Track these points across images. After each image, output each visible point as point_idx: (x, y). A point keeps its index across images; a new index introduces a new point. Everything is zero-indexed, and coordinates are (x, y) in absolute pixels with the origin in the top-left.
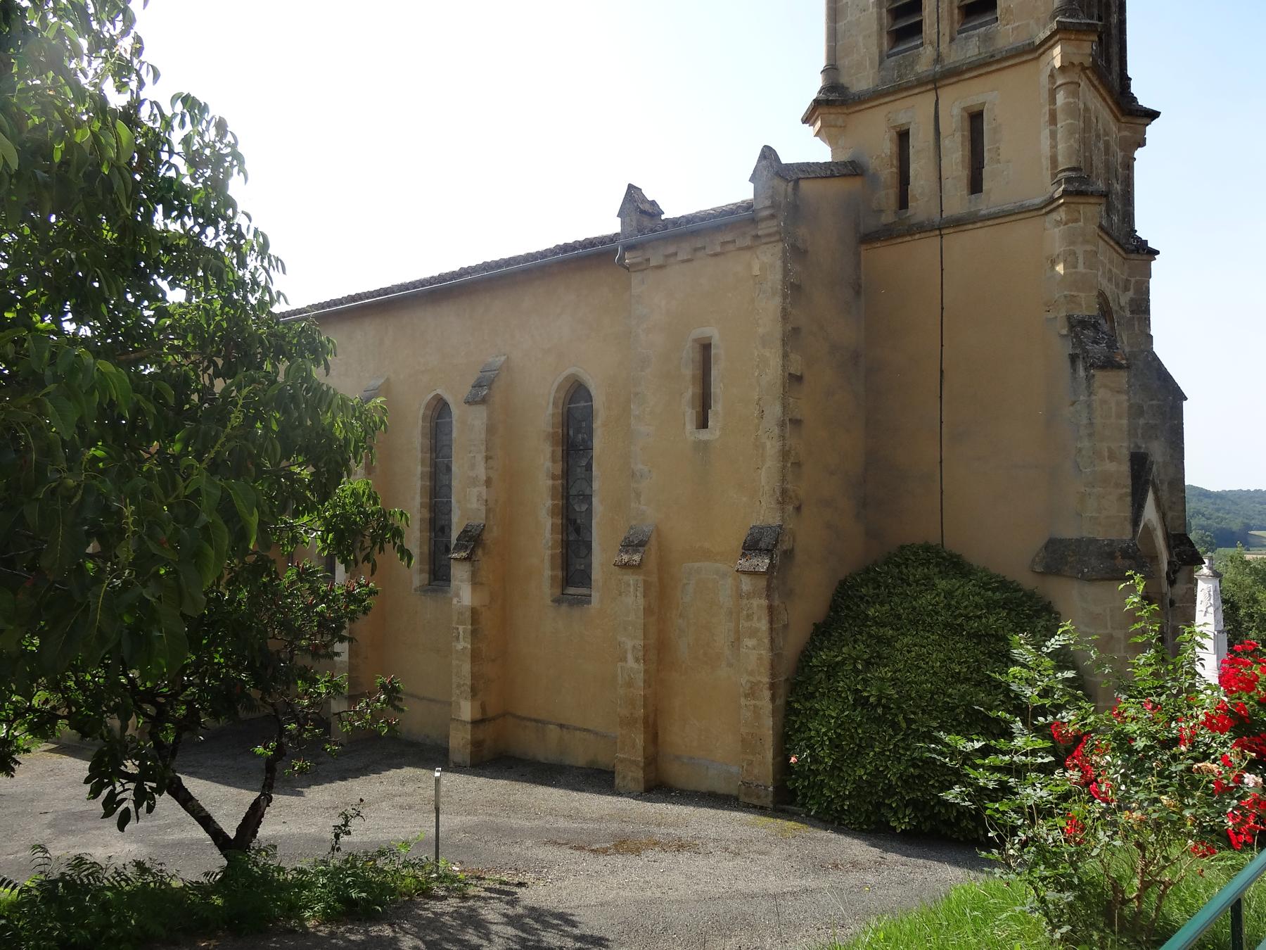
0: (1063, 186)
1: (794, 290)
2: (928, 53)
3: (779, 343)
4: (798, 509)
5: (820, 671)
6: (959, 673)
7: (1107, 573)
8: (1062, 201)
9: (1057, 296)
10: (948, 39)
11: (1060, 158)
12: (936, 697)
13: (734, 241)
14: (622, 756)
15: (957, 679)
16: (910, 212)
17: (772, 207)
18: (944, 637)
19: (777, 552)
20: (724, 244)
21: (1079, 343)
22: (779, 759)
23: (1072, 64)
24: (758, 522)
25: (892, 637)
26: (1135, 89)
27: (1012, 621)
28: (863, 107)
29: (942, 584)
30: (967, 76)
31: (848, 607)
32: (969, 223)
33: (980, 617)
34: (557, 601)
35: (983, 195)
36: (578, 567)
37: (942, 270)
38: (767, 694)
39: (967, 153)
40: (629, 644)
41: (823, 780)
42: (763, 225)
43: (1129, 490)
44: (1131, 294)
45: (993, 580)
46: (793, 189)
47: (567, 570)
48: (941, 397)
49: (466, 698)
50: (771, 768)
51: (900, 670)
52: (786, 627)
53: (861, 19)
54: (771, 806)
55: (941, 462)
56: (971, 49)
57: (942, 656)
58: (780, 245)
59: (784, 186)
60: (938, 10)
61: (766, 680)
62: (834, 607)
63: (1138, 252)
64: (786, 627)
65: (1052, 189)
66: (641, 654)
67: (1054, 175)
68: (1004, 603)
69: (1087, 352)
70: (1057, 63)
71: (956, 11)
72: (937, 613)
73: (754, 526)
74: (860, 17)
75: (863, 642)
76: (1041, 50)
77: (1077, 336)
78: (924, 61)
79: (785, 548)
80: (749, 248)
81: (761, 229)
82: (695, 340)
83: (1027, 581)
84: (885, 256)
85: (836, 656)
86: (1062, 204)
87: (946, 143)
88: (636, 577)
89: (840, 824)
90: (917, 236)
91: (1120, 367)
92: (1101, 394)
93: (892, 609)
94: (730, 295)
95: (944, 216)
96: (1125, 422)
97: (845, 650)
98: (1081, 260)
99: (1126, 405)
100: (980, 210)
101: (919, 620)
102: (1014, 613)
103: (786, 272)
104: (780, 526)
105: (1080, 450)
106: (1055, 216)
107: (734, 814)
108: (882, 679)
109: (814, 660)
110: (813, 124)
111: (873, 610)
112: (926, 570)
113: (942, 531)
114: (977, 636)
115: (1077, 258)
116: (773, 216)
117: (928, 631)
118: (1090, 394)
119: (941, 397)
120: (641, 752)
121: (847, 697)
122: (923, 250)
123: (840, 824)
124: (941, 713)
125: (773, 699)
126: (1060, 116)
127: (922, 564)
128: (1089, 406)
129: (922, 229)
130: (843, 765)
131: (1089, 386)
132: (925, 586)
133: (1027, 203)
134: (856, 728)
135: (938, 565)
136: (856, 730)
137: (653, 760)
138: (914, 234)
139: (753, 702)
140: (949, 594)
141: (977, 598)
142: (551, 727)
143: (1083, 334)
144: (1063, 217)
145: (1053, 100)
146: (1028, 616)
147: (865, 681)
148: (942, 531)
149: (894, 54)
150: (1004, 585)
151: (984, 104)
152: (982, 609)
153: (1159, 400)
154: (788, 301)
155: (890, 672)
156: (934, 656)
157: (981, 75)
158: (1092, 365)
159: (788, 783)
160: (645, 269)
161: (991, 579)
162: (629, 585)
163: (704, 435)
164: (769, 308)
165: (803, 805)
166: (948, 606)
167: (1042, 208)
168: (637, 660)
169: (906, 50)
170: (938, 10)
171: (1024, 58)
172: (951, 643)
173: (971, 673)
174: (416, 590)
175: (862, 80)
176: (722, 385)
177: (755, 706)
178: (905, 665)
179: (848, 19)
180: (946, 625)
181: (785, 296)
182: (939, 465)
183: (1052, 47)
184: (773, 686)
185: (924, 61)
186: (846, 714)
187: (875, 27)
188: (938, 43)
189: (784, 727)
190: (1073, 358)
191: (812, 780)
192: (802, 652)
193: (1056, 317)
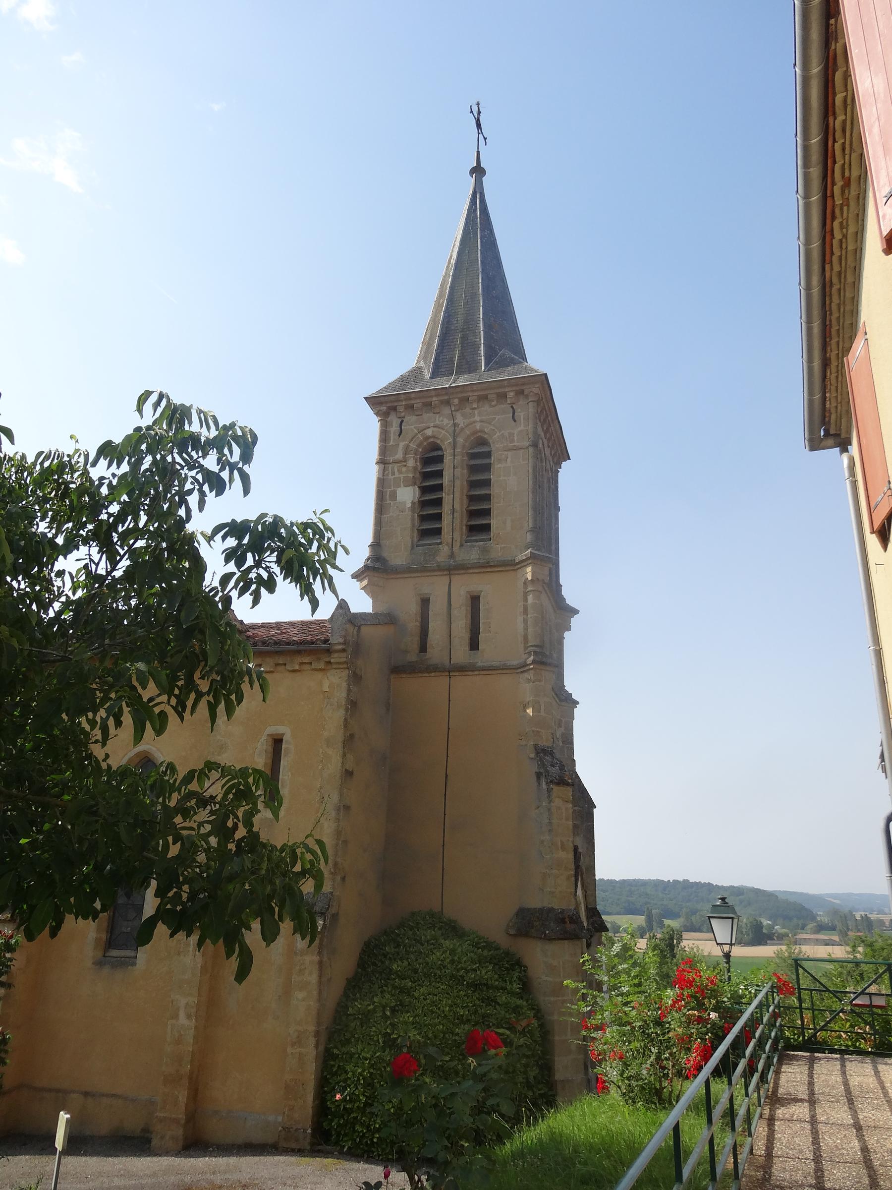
0: (532, 657)
1: (352, 705)
2: (445, 550)
3: (340, 745)
4: (343, 879)
5: (355, 1019)
6: (462, 1016)
7: (561, 934)
8: (532, 667)
9: (527, 730)
10: (459, 544)
11: (529, 637)
12: (447, 1036)
14: (162, 1115)
15: (462, 1020)
16: (428, 655)
17: (344, 643)
18: (451, 987)
19: (328, 915)
20: (302, 664)
21: (542, 765)
22: (317, 1102)
23: (538, 579)
25: (411, 988)
26: (565, 592)
27: (496, 973)
29: (447, 943)
30: (471, 571)
31: (374, 964)
32: (470, 671)
33: (475, 970)
34: (99, 964)
36: (124, 930)
38: (312, 1041)
39: (469, 622)
40: (183, 1001)
41: (355, 1118)
42: (336, 655)
43: (573, 873)
44: (562, 729)
45: (482, 940)
46: (357, 632)
47: (111, 932)
50: (311, 1110)
51: (418, 1015)
52: (329, 980)
53: (400, 517)
54: (308, 1148)
55: (443, 845)
56: (472, 554)
57: (450, 1002)
58: (346, 672)
59: (352, 630)
60: (453, 524)
61: (312, 1028)
62: (362, 964)
63: (567, 702)
64: (329, 980)
65: (526, 656)
66: (194, 1010)
67: (526, 648)
68: (491, 959)
69: (548, 771)
70: (530, 578)
71: (464, 527)
72: (444, 967)
73: (308, 893)
74: (399, 515)
75: (388, 992)
76: (519, 566)
77: (541, 760)
78: (442, 556)
79: (333, 912)
80: (322, 670)
81: (333, 658)
82: (268, 735)
83: (502, 940)
84: (411, 685)
85: (369, 1005)
86: (532, 669)
89: (368, 1157)
90: (433, 674)
91: (568, 784)
92: (557, 802)
93: (409, 964)
94: (303, 703)
96: (571, 823)
97: (376, 999)
98: (542, 707)
99: (571, 811)
100: (478, 662)
101: (432, 973)
102: (497, 967)
103: (349, 691)
104: (331, 893)
105: (542, 842)
106: (526, 675)
107: (277, 1158)
108: (406, 1023)
109: (350, 1009)
110: (361, 581)
111: (396, 966)
112: (433, 932)
113: (442, 901)
114: (476, 986)
115: (540, 706)
116: (344, 650)
117: (438, 982)
118: (550, 802)
120: (183, 1108)
121: (378, 1040)
122: (437, 684)
123: (368, 1157)
124: (451, 1050)
125: (317, 1046)
126: (530, 610)
127: (430, 928)
128: (549, 810)
129: (436, 669)
130: (374, 1101)
131: (549, 796)
132: (434, 945)
133: (508, 663)
134: (385, 1067)
135: (440, 929)
136: (385, 1069)
137: (192, 1117)
138: (431, 672)
139: (298, 1050)
140: (453, 952)
141: (472, 955)
143: (545, 759)
144: (532, 677)
145: (526, 600)
146: (507, 968)
147: (393, 1025)
148: (442, 901)
149: (423, 545)
150: (489, 945)
151: (481, 591)
152: (476, 964)
153: (579, 807)
154: (348, 714)
155: (412, 1017)
156: (444, 1002)
158: (551, 781)
159: (324, 1124)
161: (480, 939)
164: (334, 718)
165: (336, 1143)
166: (452, 962)
167: (518, 668)
168: (189, 1017)
169: (430, 544)
170: (453, 524)
171: (507, 568)
172: (455, 991)
173: (471, 1016)
175: (398, 558)
176: (290, 773)
177: (300, 1054)
178: (422, 1011)
179: (391, 514)
180: (452, 977)
181: (347, 710)
183: (526, 566)
184: (317, 1034)
185: (442, 556)
186: (377, 1055)
187: (409, 525)
188: (452, 545)
189: (322, 1072)
190: (539, 775)
191: (346, 1118)
192: (338, 1004)
193: (526, 745)
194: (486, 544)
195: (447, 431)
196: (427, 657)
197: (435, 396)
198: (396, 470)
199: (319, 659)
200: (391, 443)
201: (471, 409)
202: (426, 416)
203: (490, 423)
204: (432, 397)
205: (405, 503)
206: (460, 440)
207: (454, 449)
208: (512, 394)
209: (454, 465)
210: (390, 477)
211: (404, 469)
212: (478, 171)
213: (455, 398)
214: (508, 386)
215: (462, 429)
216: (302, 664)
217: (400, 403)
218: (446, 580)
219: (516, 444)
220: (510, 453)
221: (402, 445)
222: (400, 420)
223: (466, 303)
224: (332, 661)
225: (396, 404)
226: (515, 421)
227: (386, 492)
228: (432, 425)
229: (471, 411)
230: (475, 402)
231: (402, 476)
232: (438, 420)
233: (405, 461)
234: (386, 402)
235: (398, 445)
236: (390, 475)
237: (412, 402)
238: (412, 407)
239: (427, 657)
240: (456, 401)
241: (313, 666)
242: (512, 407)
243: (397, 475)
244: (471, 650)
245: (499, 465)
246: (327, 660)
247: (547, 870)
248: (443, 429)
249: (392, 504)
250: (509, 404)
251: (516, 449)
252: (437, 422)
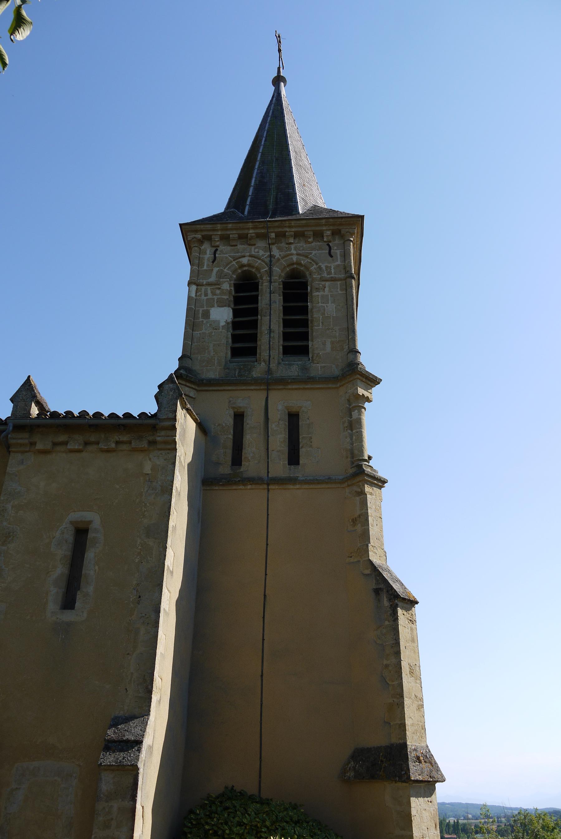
10: (276, 361)
13: (130, 443)
24: (122, 712)
28: (211, 388)
30: (290, 387)
35: (300, 467)
37: (268, 515)
48: (264, 617)
53: (213, 334)
55: (262, 676)
71: (281, 347)
82: (71, 523)
87: (272, 426)
94: (118, 487)
95: (270, 476)
119: (264, 617)
151: (301, 407)
157: (299, 389)
160: (26, 452)
163: (68, 616)
176: (97, 567)
182: (260, 678)
185: (259, 370)
193: (359, 561)
194: (305, 363)
195: (263, 261)
196: (242, 470)
197: (252, 228)
198: (209, 292)
200: (205, 268)
201: (287, 244)
203: (307, 257)
204: (248, 229)
205: (219, 322)
207: (270, 277)
208: (329, 233)
209: (271, 291)
210: (203, 297)
211: (218, 292)
212: (278, 80)
213: (272, 232)
214: (325, 225)
215: (278, 260)
216: (117, 443)
217: (215, 233)
218: (263, 394)
219: (333, 276)
220: (327, 284)
221: (216, 270)
222: (214, 249)
224: (159, 439)
225: (211, 233)
226: (331, 256)
227: (199, 310)
228: (248, 254)
229: (287, 246)
230: (292, 237)
231: (215, 297)
233: (219, 285)
234: (202, 231)
235: (212, 270)
236: (203, 296)
237: (228, 232)
239: (242, 470)
240: (273, 235)
241: (133, 444)
242: (328, 245)
243: (210, 296)
244: (290, 464)
245: (317, 293)
246: (151, 438)
247: (395, 700)
248: (259, 259)
249: (205, 322)
250: (325, 242)
251: (333, 280)
252: (253, 253)
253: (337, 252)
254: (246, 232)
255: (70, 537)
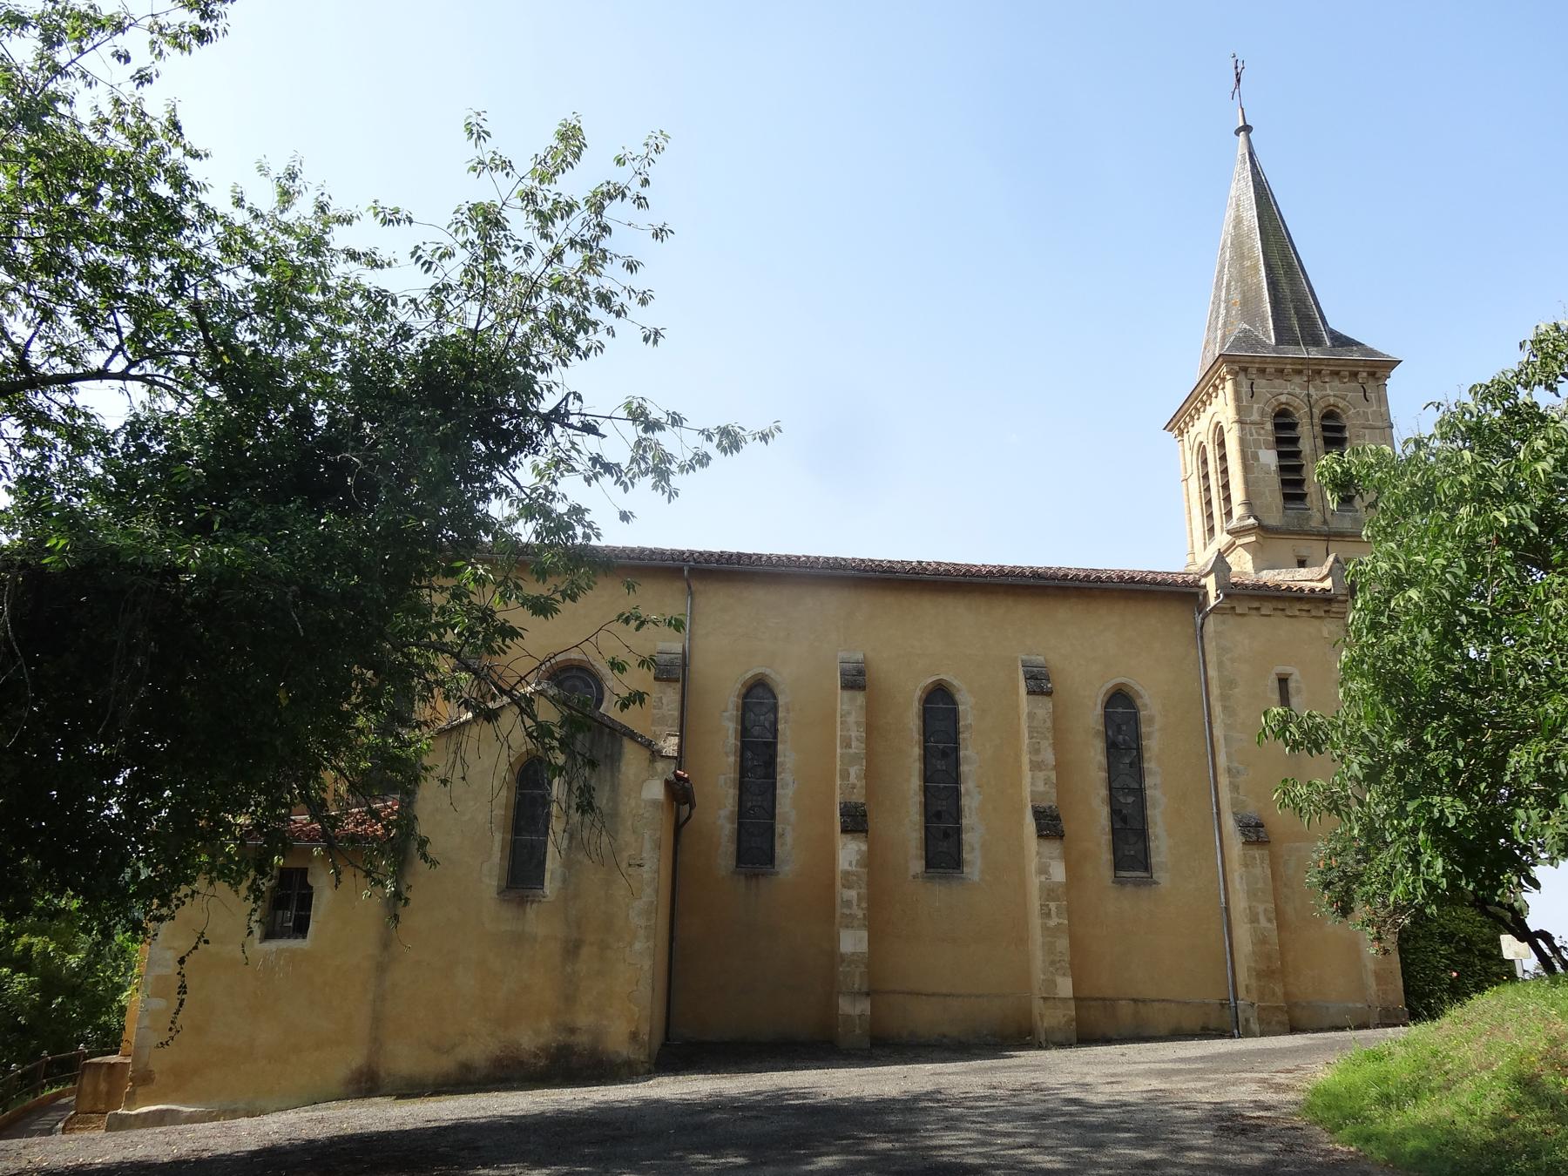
36: (1127, 853)
42: (1336, 605)
49: (1064, 975)
66: (1273, 915)
88: (1263, 852)
142: (1123, 1002)
162: (1255, 858)
168: (1269, 920)
174: (914, 877)
199: (1318, 608)
202: (1277, 382)
206: (1316, 411)
211: (1262, 432)
215: (1317, 401)
220: (1367, 431)
223: (1286, 273)
228: (1286, 391)
232: (1290, 388)
238: (1282, 371)
241: (1314, 613)
243: (1255, 436)
246: (1327, 608)
253: (1372, 395)
254: (1283, 367)
255: (1276, 684)
